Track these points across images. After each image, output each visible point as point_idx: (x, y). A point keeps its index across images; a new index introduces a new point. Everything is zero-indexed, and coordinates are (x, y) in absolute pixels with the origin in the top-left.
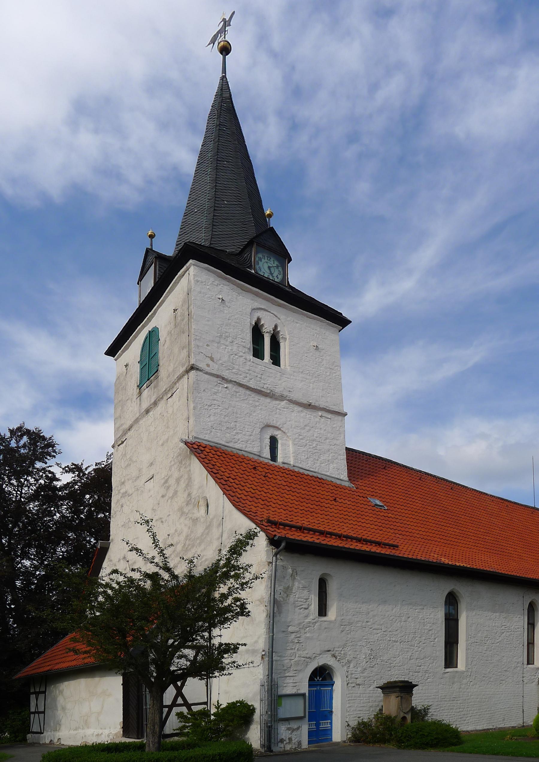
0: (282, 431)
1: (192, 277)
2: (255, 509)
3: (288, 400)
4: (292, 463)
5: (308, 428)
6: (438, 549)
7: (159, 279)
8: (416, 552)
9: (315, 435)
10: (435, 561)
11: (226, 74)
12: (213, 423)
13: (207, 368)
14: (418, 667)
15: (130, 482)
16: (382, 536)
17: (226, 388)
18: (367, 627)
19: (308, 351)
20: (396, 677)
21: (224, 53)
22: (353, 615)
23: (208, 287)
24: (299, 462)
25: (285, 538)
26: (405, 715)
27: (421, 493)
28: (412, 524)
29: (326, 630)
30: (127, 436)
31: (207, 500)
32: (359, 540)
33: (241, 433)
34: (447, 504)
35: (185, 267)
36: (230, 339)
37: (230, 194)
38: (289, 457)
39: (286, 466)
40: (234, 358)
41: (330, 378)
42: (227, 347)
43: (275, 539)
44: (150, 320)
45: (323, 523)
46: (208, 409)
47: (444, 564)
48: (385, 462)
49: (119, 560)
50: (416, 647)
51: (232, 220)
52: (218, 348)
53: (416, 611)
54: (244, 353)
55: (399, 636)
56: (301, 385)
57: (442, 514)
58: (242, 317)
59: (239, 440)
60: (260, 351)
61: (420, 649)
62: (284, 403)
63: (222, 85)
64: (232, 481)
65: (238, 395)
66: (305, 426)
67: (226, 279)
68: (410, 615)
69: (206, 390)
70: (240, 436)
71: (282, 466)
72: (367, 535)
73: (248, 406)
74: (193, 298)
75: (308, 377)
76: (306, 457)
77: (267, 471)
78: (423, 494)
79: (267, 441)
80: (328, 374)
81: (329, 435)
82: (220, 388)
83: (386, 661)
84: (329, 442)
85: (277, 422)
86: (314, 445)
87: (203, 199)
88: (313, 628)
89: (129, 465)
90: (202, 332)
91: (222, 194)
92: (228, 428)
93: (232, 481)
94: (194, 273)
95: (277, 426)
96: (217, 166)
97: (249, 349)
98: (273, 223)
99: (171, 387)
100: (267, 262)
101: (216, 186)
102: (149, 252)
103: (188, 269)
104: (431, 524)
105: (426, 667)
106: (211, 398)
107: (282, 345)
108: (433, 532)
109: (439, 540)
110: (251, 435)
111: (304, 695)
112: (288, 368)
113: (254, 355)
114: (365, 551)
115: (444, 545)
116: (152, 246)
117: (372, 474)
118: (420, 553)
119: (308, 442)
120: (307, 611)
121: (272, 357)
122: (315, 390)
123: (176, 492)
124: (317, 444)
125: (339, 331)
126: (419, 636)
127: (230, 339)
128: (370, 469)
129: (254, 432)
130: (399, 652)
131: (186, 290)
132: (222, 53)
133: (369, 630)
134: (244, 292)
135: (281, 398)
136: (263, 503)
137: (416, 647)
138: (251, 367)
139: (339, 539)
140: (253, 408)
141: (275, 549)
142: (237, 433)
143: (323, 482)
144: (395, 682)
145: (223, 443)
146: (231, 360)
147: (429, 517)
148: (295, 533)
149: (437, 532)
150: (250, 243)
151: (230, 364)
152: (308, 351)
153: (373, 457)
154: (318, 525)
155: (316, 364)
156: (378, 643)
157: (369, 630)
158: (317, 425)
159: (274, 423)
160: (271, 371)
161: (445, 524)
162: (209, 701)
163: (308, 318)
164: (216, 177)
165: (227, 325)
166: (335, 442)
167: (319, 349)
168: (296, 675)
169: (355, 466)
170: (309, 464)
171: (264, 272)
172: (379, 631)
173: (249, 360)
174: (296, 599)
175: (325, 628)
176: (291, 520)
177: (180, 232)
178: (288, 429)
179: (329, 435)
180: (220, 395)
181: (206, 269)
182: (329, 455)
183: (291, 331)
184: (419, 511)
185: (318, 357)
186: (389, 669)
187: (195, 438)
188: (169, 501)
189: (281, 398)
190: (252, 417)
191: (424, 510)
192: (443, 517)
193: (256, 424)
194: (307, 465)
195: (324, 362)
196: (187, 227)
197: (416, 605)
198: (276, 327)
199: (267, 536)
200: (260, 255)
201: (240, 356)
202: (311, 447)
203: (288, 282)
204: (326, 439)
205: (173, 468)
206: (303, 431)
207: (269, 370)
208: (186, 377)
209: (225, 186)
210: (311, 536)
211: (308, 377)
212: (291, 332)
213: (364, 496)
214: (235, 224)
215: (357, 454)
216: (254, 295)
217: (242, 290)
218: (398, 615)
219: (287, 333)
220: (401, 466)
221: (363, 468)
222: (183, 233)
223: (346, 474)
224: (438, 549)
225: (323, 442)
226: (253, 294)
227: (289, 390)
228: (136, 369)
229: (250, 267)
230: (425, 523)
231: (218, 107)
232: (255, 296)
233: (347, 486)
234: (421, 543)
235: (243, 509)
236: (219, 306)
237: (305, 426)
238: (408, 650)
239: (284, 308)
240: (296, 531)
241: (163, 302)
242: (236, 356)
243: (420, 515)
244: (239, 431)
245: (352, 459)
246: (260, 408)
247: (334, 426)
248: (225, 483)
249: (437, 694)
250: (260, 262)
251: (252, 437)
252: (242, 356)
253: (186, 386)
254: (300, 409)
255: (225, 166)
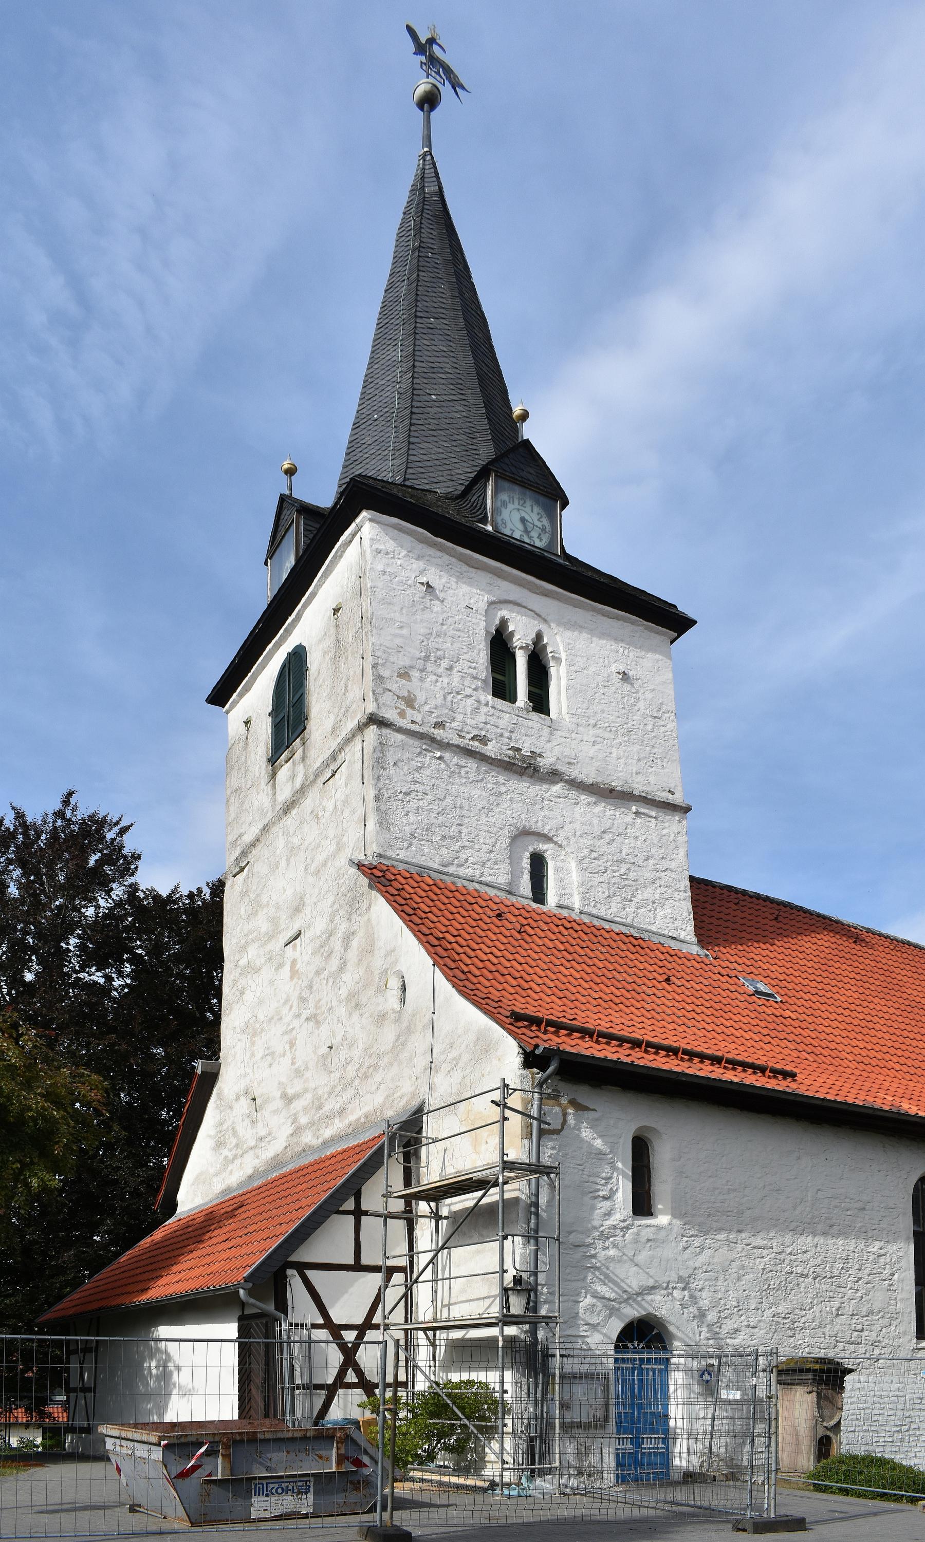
0: (556, 843)
1: (366, 542)
2: (498, 994)
3: (566, 781)
4: (577, 905)
5: (608, 837)
6: (895, 1085)
7: (305, 551)
8: (845, 1089)
9: (624, 852)
10: (886, 1108)
11: (430, 149)
12: (414, 827)
13: (400, 720)
14: (856, 1333)
15: (256, 945)
16: (771, 1054)
17: (440, 758)
18: (739, 1242)
19: (606, 684)
20: (807, 1350)
21: (426, 106)
22: (709, 1216)
23: (399, 562)
24: (592, 904)
25: (557, 1053)
26: (828, 1433)
27: (857, 970)
28: (836, 1032)
29: (649, 1244)
30: (250, 858)
31: (403, 977)
32: (716, 1060)
33: (471, 847)
34: (915, 993)
35: (353, 526)
36: (445, 664)
37: (443, 381)
38: (571, 895)
39: (565, 913)
40: (455, 700)
41: (655, 737)
42: (440, 679)
43: (537, 1052)
44: (288, 632)
45: (640, 1026)
46: (403, 801)
47: (906, 1114)
48: (778, 907)
49: (238, 1099)
50: (851, 1289)
51: (447, 432)
52: (422, 681)
53: (849, 1213)
54: (475, 690)
55: (811, 1263)
56: (592, 752)
57: (905, 1014)
58: (469, 619)
59: (467, 860)
60: (507, 686)
61: (859, 1294)
62: (557, 788)
63: (424, 169)
64: (453, 939)
65: (463, 773)
66: (604, 832)
67: (434, 545)
68: (834, 1221)
69: (400, 764)
70: (468, 853)
71: (556, 912)
72: (736, 1052)
73: (484, 794)
74: (369, 585)
75: (607, 735)
76: (607, 894)
77: (525, 922)
78: (863, 972)
79: (526, 863)
80: (649, 727)
81: (653, 851)
82: (427, 759)
83: (783, 1315)
84: (655, 865)
85: (543, 825)
86: (623, 871)
87: (389, 393)
88: (621, 1239)
89: (254, 914)
90: (390, 651)
91: (425, 381)
92: (444, 837)
93: (453, 939)
94: (370, 536)
95: (546, 830)
96: (415, 327)
97: (484, 681)
98: (528, 431)
99: (334, 757)
100: (518, 510)
101: (414, 366)
102: (284, 500)
103: (359, 529)
104: (880, 1034)
105: (874, 1334)
106: (410, 778)
107: (553, 671)
108: (885, 1049)
109: (898, 1067)
110: (491, 852)
111: (604, 1377)
112: (567, 717)
113: (495, 694)
114: (731, 1083)
115: (908, 1077)
116: (291, 490)
117: (750, 930)
118: (854, 1091)
119: (609, 864)
120: (608, 1204)
121: (532, 696)
122: (622, 761)
123: (343, 964)
124: (629, 869)
125: (672, 643)
126: (857, 1266)
127: (445, 664)
128: (743, 921)
129: (498, 844)
130: (813, 1299)
131: (355, 570)
132: (422, 109)
133: (743, 1248)
134: (471, 569)
135: (554, 776)
136: (514, 983)
137: (851, 1289)
138: (489, 718)
139: (673, 1057)
140: (495, 798)
141: (538, 1073)
142: (463, 847)
143: (644, 945)
144: (805, 1360)
145: (436, 866)
146: (449, 704)
147: (875, 1019)
148: (579, 1042)
149: (892, 1051)
150: (482, 475)
151: (447, 711)
152: (606, 684)
153: (751, 897)
154: (630, 1030)
155: (624, 708)
156: (764, 1277)
157: (743, 1248)
158: (628, 830)
159: (539, 827)
160: (530, 723)
161: (911, 1035)
162: (410, 1379)
163: (605, 618)
164: (414, 350)
165: (438, 636)
166: (666, 864)
167: (629, 678)
168: (588, 1333)
169: (712, 914)
170: (613, 910)
171: (514, 528)
172: (765, 1252)
173: (484, 702)
174: (586, 1178)
175: (649, 1240)
176: (572, 1017)
177: (346, 461)
178: (568, 838)
179: (653, 851)
180: (428, 772)
181: (395, 527)
182: (656, 890)
183: (569, 644)
184: (852, 1007)
185: (628, 695)
186: (790, 1333)
187: (380, 856)
188: (331, 980)
189: (554, 776)
190: (493, 816)
191: (865, 1004)
192: (907, 1021)
193: (501, 829)
194: (610, 912)
195: (641, 704)
196: (359, 450)
197: (848, 1200)
198: (539, 636)
199: (520, 1047)
200: (504, 496)
201: (467, 696)
202: (617, 874)
203: (562, 547)
204: (648, 858)
205: (337, 918)
206: (598, 843)
207: (526, 722)
208: (359, 738)
209: (433, 365)
210: (614, 1050)
211: (607, 735)
212: (570, 646)
213: (732, 974)
214: (452, 438)
215: (717, 889)
216: (491, 575)
217: (468, 565)
218: (808, 1221)
219: (561, 647)
220: (812, 915)
221: (728, 918)
222: (350, 462)
223: (691, 928)
224: (895, 1085)
225: (640, 863)
226: (490, 573)
227: (567, 760)
228: (264, 729)
229: (484, 520)
230: (865, 1031)
231: (417, 213)
232: (495, 577)
233: (694, 953)
234: (857, 1072)
235: (472, 993)
236: (423, 598)
237: (604, 832)
238: (832, 1294)
239: (554, 598)
240: (582, 1038)
241: (314, 595)
242: (459, 697)
243: (854, 1014)
244: (467, 844)
245: (706, 899)
246: (509, 797)
247: (665, 832)
248: (436, 942)
249: (901, 1394)
250: (503, 510)
251: (493, 856)
252: (470, 696)
253: (358, 755)
254: (592, 799)
255: (431, 326)
